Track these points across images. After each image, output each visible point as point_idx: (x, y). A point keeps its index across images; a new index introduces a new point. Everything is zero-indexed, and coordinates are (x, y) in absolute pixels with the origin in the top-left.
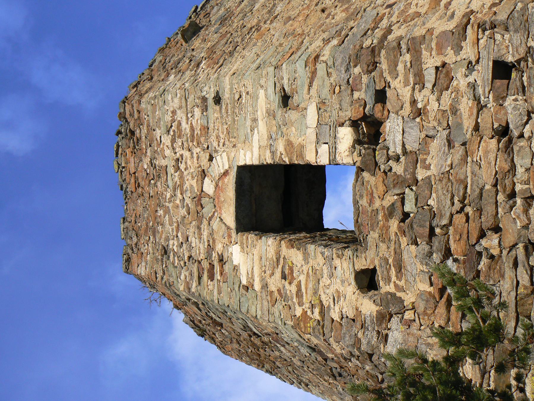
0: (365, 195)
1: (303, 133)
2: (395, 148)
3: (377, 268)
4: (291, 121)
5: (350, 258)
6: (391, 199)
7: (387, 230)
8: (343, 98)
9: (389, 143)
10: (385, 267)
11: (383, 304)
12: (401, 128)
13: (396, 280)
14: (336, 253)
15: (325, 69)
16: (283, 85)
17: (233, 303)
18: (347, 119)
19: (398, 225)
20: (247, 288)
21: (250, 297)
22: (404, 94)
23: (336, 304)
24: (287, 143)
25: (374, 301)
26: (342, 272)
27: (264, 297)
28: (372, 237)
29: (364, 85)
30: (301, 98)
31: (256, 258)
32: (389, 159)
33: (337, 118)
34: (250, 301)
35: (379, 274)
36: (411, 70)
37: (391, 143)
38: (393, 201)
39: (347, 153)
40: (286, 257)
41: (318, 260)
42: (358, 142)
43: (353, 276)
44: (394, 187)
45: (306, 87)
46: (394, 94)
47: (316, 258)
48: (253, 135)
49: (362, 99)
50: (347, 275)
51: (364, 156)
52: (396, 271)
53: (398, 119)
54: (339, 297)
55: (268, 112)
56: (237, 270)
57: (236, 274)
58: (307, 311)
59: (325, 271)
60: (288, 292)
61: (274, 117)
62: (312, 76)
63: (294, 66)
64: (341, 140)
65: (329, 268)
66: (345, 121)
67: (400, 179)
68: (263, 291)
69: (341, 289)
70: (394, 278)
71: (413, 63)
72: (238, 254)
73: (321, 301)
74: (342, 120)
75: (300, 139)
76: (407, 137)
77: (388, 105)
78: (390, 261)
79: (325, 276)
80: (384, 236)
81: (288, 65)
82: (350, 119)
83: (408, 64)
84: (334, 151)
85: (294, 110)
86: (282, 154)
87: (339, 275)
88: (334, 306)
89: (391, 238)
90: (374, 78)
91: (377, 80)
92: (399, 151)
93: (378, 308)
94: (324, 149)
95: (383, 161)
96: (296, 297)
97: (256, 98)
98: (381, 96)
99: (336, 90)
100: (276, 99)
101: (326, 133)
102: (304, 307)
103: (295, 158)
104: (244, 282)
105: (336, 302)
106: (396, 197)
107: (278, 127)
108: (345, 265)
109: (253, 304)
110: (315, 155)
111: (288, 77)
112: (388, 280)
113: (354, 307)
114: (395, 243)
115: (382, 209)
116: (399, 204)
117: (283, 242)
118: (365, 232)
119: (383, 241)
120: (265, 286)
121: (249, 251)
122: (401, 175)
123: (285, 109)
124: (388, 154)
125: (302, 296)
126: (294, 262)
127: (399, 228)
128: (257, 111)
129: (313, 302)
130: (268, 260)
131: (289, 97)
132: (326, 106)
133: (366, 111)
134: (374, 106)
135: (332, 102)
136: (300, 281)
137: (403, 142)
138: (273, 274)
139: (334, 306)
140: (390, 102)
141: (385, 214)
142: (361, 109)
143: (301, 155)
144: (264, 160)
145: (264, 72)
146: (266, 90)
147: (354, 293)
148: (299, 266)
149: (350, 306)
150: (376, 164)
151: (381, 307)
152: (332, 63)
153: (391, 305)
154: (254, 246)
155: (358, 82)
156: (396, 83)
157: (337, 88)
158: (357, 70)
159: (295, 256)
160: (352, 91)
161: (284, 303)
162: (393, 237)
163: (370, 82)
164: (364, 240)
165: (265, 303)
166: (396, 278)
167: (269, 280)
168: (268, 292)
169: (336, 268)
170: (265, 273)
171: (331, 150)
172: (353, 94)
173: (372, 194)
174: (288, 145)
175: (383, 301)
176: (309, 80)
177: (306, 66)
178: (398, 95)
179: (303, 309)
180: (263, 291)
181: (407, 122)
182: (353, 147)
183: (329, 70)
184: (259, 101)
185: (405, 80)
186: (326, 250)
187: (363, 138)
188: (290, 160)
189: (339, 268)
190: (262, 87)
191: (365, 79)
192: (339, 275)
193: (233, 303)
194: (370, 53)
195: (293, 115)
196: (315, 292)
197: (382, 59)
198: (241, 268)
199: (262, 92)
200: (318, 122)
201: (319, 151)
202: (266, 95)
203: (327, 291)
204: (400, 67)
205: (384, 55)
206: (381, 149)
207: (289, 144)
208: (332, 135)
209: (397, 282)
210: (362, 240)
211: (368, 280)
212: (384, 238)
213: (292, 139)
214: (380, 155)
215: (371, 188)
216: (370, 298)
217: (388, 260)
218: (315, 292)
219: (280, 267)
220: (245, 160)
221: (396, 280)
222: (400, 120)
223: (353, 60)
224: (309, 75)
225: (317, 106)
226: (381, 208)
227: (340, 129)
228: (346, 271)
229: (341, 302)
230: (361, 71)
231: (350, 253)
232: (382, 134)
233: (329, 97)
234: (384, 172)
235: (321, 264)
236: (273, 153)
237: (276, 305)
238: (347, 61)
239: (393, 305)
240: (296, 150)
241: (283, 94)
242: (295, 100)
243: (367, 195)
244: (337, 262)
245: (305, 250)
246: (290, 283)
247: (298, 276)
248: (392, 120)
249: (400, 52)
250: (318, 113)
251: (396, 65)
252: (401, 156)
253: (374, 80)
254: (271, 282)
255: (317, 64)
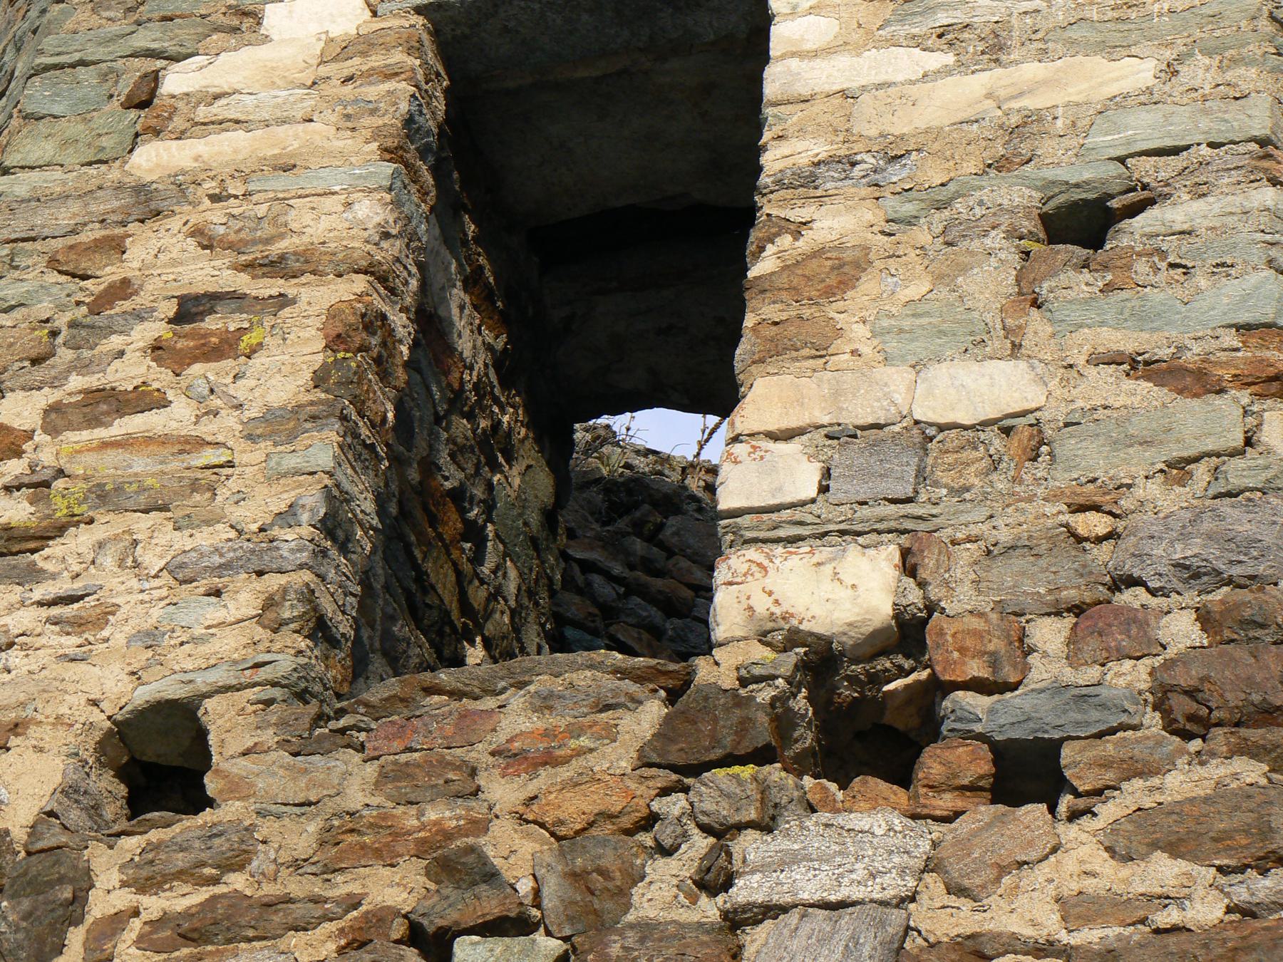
0: (552, 720)
1: (892, 345)
2: (761, 868)
3: (207, 816)
4: (964, 269)
5: (257, 666)
6: (519, 857)
7: (378, 853)
8: (1043, 562)
9: (787, 834)
10: (204, 856)
11: (37, 865)
12: (857, 893)
13: (145, 916)
14: (284, 590)
15: (1210, 446)
16: (1167, 196)
17: (69, 25)
18: (934, 592)
19: (397, 913)
20: (144, 98)
21: (99, 121)
22: (1022, 900)
23: (45, 612)
24: (848, 256)
25: (51, 814)
26: (199, 631)
27: (97, 208)
28: (347, 774)
29: (1093, 673)
30: (1076, 316)
31: (291, 139)
32: (721, 832)
33: (944, 535)
34: (74, 128)
35: (177, 828)
36: (1137, 933)
37: (786, 844)
38: (508, 875)
39: (762, 605)
40: (286, 312)
41: (262, 491)
42: (820, 660)
43: (170, 689)
44: (575, 876)
45: (1127, 342)
46: (1030, 843)
47: (269, 479)
48: (917, 42)
49: (1026, 669)
50: (183, 659)
51: (740, 702)
52: (187, 914)
53: (902, 872)
54: (78, 625)
55: (1025, 127)
56: (235, 30)
57: (218, 29)
58: (19, 454)
59: (205, 538)
60: (116, 341)
61: (1000, 165)
62: (1182, 371)
63: (1257, 255)
64: (828, 569)
65: (217, 560)
66: (922, 585)
67: (609, 905)
68: (126, 199)
69: (117, 633)
70: (153, 905)
71: (1172, 939)
72: (314, 28)
73: (60, 530)
74: (929, 563)
75: (861, 331)
76: (806, 928)
77: (983, 812)
78: (237, 882)
79: (182, 541)
80: (350, 838)
81: (1264, 219)
82: (931, 607)
83: (1171, 916)
84: (782, 533)
85: (1018, 281)
86: (797, 230)
87: (183, 618)
88: (40, 604)
89: (339, 878)
90: (1123, 727)
91: (1109, 747)
92: (747, 890)
93: (19, 834)
94: (796, 475)
95: (708, 806)
96: (87, 392)
97: (1116, 38)
98: (1027, 773)
99: (1092, 516)
100: (1075, 167)
101: (894, 479)
102: (39, 437)
103: (771, 311)
104: (176, 81)
105: (56, 611)
106: (525, 886)
107: (944, 194)
108: (229, 644)
109: (65, 143)
110: (772, 426)
111: (1201, 224)
112: (147, 879)
113: (29, 712)
114: (316, 900)
115: (473, 822)
116: (490, 905)
117: (360, 283)
118: (379, 736)
119: (328, 838)
120: (148, 205)
121: (327, 89)
122: (628, 907)
123: (1027, 225)
124: (740, 827)
125: (94, 422)
126: (259, 361)
127: (381, 917)
128: (1042, 56)
129: (59, 484)
130: (277, 207)
131: (1095, 242)
132: (1018, 467)
133: (960, 693)
134: (981, 737)
135: (1030, 500)
136: (164, 404)
137: (784, 909)
138: (207, 242)
139: (40, 604)
140: (989, 825)
141: (449, 836)
142: (976, 669)
143: (777, 350)
144: (777, 130)
145: (1247, 77)
146: (1148, 98)
147: (95, 703)
148: (240, 391)
149: (33, 689)
150: (696, 770)
151: (23, 854)
152: (1235, 482)
153: (26, 904)
154: (349, 122)
155: (1119, 638)
156: (1083, 851)
157: (1095, 523)
158: (1181, 630)
159: (285, 364)
160: (1078, 610)
161: (61, 321)
162: (343, 886)
163: (1103, 706)
164: (342, 731)
165: (65, 216)
166: (155, 915)
167: (175, 224)
168: (124, 224)
169: (217, 593)
170: (215, 198)
171: (786, 514)
172: (1058, 614)
173: (549, 760)
174: (839, 266)
175: (48, 860)
176: (1164, 353)
177: (1244, 329)
178: (1021, 864)
179: (29, 435)
180: (126, 199)
181: (882, 924)
182: (794, 638)
183: (1201, 472)
184: (1098, 63)
185: (1095, 900)
186: (306, 531)
187: (853, 680)
188: (766, 286)
189: (214, 612)
190: (1171, 71)
191: (1132, 676)
192: (183, 618)
193: (69, 25)
194: (1256, 698)
195: (990, 278)
196: (105, 496)
197: (1217, 770)
198: (247, 54)
199: (1138, 72)
200: (942, 428)
201: (791, 448)
202: (1119, 102)
203: (108, 561)
204: (1164, 871)
205: (1235, 776)
206: (764, 789)
207: (841, 271)
208: (865, 512)
209: (136, 924)
210: (342, 723)
211: (177, 762)
212: (347, 841)
213: (868, 285)
214: (734, 788)
215: (580, 752)
216: (69, 791)
217: (241, 868)
218: (105, 496)
219: (243, 283)
220: (794, 12)
221: (145, 916)
222: (893, 885)
223: (1238, 606)
224: (1190, 359)
225: (1023, 414)
226: (477, 808)
227: (889, 553)
228: (204, 649)
229: (56, 640)
230: (1171, 652)
231: (285, 664)
232: (843, 787)
233: (1061, 479)
234: (651, 820)
235: (238, 513)
236: (806, 182)
237: (53, 277)
238: (1236, 571)
239: (27, 916)
240: (807, 312)
241: (1114, 204)
242: (1072, 283)
243: (547, 734)
244: (244, 596)
245: (314, 418)
246: (157, 348)
247: (187, 392)
248: (898, 841)
249: (1242, 869)
250: (985, 424)
251: (1175, 849)
252: (720, 899)
253: (1113, 731)
254: (167, 240)
255: (1244, 397)
